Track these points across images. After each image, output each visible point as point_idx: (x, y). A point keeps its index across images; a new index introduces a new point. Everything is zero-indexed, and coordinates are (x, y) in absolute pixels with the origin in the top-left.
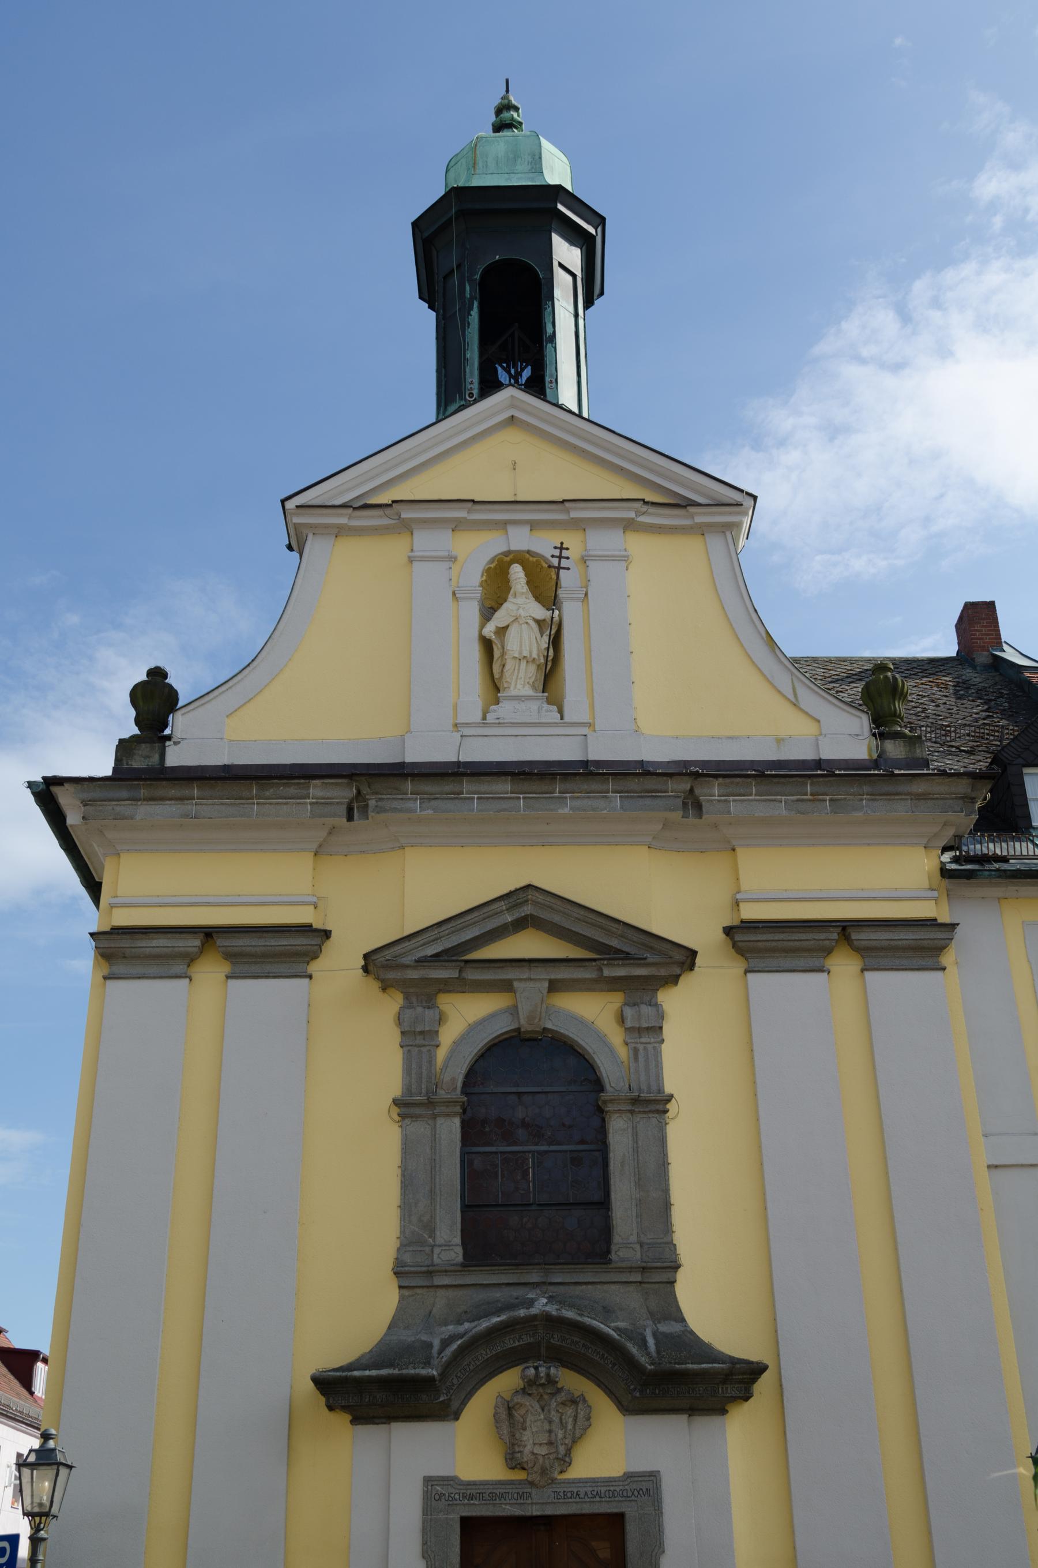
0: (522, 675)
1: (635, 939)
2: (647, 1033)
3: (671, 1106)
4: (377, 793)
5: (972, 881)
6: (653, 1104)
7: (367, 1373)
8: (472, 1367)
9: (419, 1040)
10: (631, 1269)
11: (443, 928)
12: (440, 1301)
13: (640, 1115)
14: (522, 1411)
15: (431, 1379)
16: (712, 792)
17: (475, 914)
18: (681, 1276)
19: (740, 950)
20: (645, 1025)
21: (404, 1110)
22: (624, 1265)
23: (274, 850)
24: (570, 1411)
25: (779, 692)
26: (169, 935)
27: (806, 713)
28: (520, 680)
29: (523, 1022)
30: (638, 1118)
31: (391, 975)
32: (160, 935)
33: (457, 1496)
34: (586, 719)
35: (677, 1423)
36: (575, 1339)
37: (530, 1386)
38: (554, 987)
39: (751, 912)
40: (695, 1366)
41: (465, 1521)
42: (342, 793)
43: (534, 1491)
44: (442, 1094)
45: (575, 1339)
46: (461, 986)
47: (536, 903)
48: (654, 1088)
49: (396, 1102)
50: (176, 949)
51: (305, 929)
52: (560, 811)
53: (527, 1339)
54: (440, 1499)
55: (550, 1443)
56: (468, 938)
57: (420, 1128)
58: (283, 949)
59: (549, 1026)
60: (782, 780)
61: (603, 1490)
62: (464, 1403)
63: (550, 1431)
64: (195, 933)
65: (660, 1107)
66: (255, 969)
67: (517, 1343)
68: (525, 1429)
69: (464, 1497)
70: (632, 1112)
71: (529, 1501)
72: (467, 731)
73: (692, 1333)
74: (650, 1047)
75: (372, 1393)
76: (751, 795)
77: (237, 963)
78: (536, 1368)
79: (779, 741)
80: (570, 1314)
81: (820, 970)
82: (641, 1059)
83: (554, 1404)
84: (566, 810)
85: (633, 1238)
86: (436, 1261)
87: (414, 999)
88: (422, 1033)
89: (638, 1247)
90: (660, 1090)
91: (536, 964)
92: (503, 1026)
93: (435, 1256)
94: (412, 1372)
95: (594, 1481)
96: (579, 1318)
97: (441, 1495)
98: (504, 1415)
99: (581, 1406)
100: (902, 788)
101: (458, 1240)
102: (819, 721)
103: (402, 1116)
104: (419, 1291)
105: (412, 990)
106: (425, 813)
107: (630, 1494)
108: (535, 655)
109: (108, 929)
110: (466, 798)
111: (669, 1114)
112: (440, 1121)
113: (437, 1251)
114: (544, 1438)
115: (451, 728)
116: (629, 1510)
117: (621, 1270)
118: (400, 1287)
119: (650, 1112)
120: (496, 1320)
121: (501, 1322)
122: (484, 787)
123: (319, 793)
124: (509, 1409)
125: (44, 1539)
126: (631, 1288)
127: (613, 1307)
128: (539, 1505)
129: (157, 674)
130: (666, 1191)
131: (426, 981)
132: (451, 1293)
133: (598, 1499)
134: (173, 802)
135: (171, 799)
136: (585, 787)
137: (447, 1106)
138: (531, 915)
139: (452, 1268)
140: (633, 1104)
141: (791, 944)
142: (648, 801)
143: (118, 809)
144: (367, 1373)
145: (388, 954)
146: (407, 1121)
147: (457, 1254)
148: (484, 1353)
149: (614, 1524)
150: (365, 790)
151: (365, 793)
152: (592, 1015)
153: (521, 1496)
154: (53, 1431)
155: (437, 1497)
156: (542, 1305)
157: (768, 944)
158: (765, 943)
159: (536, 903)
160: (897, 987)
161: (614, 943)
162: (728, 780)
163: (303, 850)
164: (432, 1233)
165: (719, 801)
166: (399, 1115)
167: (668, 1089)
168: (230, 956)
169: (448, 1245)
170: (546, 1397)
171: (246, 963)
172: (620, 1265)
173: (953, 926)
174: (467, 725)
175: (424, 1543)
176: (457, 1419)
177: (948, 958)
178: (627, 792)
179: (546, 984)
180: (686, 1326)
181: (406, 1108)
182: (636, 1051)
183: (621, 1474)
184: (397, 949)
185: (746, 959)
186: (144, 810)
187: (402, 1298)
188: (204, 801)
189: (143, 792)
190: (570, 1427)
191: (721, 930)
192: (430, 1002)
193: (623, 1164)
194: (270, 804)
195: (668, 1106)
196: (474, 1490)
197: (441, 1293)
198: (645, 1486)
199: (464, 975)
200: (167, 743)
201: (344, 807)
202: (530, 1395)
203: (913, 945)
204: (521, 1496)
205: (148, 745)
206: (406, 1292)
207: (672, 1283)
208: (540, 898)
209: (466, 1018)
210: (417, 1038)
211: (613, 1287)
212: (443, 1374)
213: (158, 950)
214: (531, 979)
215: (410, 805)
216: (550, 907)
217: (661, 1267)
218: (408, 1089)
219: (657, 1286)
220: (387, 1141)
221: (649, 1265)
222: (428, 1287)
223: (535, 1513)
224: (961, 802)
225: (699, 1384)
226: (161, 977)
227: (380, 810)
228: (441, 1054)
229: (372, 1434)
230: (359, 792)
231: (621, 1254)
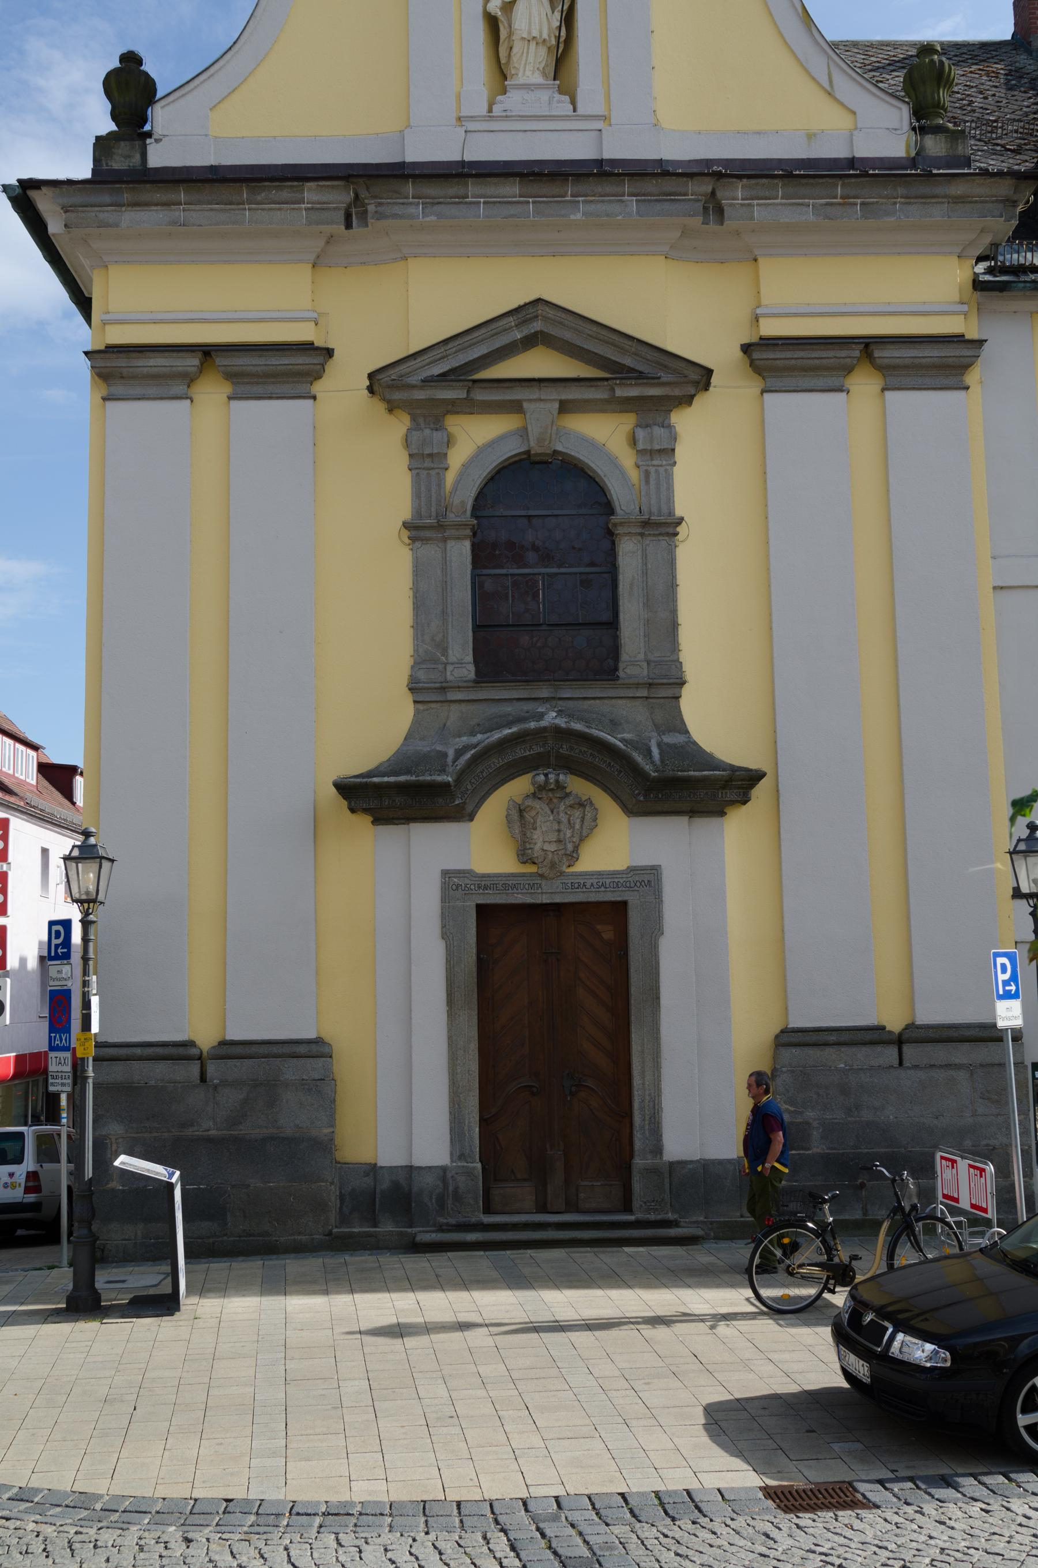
0: (531, 59)
1: (649, 357)
2: (659, 455)
3: (682, 529)
4: (376, 197)
5: (1005, 293)
6: (663, 527)
7: (386, 779)
8: (485, 774)
9: (428, 463)
10: (638, 685)
11: (450, 346)
12: (453, 715)
13: (650, 538)
14: (533, 813)
15: (447, 785)
16: (734, 195)
17: (483, 331)
18: (686, 692)
19: (757, 368)
20: (657, 447)
21: (414, 533)
22: (631, 681)
23: (270, 262)
24: (577, 813)
25: (814, 79)
26: (167, 354)
27: (842, 104)
28: (530, 64)
29: (532, 444)
30: (647, 541)
31: (397, 396)
32: (157, 354)
33: (472, 887)
34: (601, 111)
35: (681, 822)
36: (583, 749)
37: (539, 792)
38: (565, 407)
39: (771, 328)
40: (697, 773)
41: (481, 909)
42: (339, 197)
43: (544, 883)
44: (452, 517)
45: (583, 749)
46: (469, 407)
47: (546, 319)
48: (665, 510)
49: (406, 525)
50: (174, 369)
51: (307, 347)
52: (572, 217)
53: (537, 749)
54: (457, 889)
55: (559, 841)
56: (476, 356)
57: (431, 552)
58: (284, 369)
59: (560, 448)
60: (811, 181)
61: (608, 881)
62: (478, 806)
63: (559, 831)
64: (193, 351)
65: (671, 530)
66: (258, 389)
67: (528, 753)
68: (535, 829)
69: (479, 888)
70: (642, 535)
71: (539, 891)
72: (471, 126)
73: (695, 743)
74: (661, 469)
75: (392, 797)
76: (777, 198)
77: (239, 383)
78: (546, 775)
79: (811, 136)
80: (578, 726)
81: (840, 389)
82: (652, 482)
83: (562, 807)
84: (579, 216)
85: (641, 656)
86: (449, 677)
87: (421, 421)
88: (430, 455)
89: (645, 664)
90: (671, 513)
91: (546, 384)
92: (512, 449)
93: (448, 673)
94: (429, 778)
95: (600, 874)
96: (587, 730)
97: (458, 886)
98: (515, 816)
99: (588, 808)
100: (939, 190)
101: (470, 658)
102: (854, 113)
103: (413, 539)
104: (433, 705)
105: (418, 411)
106: (427, 219)
107: (632, 885)
108: (545, 36)
109: (102, 348)
110: (471, 203)
111: (678, 537)
112: (450, 544)
113: (449, 668)
114: (553, 837)
115: (454, 122)
116: (633, 899)
117: (628, 686)
118: (415, 702)
119: (660, 534)
120: (507, 731)
121: (512, 733)
122: (491, 190)
123: (315, 198)
124: (521, 811)
125: (94, 922)
126: (638, 703)
127: (619, 719)
128: (548, 894)
129: (131, 60)
130: (674, 612)
131: (433, 402)
132: (464, 707)
133: (603, 889)
134: (159, 208)
135: (157, 205)
136: (599, 189)
137: (457, 529)
138: (542, 332)
139: (465, 684)
140: (643, 527)
141: (811, 362)
142: (666, 206)
143: (101, 216)
144: (386, 779)
145: (393, 373)
146: (418, 544)
147: (469, 672)
148: (496, 762)
149: (621, 908)
150: (363, 194)
151: (366, 195)
152: (603, 437)
153: (532, 886)
154: (93, 830)
155: (454, 887)
156: (551, 718)
157: (787, 362)
158: (784, 361)
159: (546, 319)
160: (918, 407)
161: (628, 361)
162: (753, 181)
163: (300, 261)
164: (445, 651)
165: (742, 205)
166: (409, 538)
167: (679, 512)
168: (232, 376)
169: (460, 663)
170: (555, 800)
171: (247, 383)
172: (627, 681)
173: (980, 343)
174: (472, 118)
175: (443, 927)
176: (472, 820)
177: (972, 378)
178: (644, 195)
179: (557, 405)
180: (690, 737)
181: (416, 531)
182: (647, 474)
183: (625, 868)
184: (403, 368)
185: (764, 379)
186: (129, 217)
187: (417, 712)
188: (192, 207)
189: (126, 197)
190: (577, 827)
191: (739, 348)
192: (438, 424)
193: (632, 585)
194: (263, 209)
195: (678, 529)
196: (486, 882)
197: (454, 707)
198: (648, 879)
199: (472, 395)
200: (148, 141)
201: (343, 212)
202: (540, 799)
203: (936, 362)
204: (532, 886)
205: (127, 143)
206: (421, 707)
207: (677, 698)
208: (551, 313)
209: (475, 440)
210: (426, 461)
211: (620, 702)
212: (458, 780)
213: (156, 369)
214: (541, 400)
215: (412, 210)
216: (561, 323)
217: (666, 683)
218: (417, 512)
219: (662, 701)
220: (400, 560)
221: (656, 681)
222: (441, 702)
223: (544, 902)
224: (1001, 205)
225: (699, 789)
226: (162, 398)
227: (380, 216)
228: (450, 477)
229: (392, 834)
230: (357, 196)
231: (628, 671)
